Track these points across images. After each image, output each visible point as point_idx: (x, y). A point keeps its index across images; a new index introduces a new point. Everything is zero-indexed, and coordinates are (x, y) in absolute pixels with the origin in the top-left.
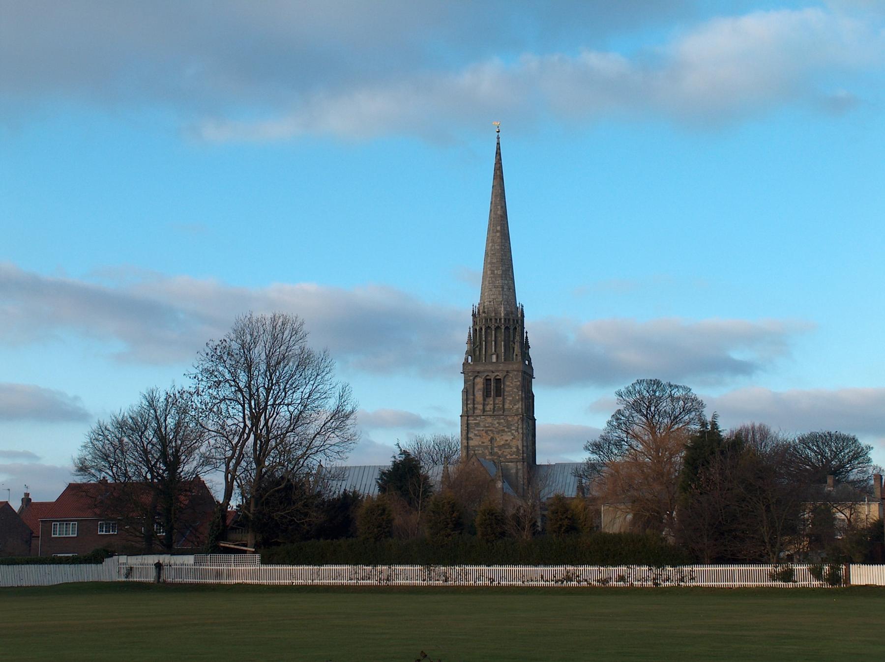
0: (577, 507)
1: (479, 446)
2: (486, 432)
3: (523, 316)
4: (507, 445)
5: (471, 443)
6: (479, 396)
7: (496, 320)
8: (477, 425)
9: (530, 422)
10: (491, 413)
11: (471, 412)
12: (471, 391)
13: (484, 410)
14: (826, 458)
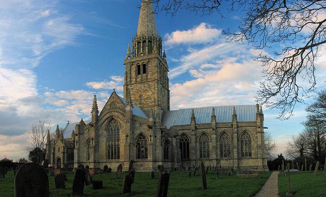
6: (133, 74)
11: (128, 83)
12: (129, 72)
13: (136, 81)
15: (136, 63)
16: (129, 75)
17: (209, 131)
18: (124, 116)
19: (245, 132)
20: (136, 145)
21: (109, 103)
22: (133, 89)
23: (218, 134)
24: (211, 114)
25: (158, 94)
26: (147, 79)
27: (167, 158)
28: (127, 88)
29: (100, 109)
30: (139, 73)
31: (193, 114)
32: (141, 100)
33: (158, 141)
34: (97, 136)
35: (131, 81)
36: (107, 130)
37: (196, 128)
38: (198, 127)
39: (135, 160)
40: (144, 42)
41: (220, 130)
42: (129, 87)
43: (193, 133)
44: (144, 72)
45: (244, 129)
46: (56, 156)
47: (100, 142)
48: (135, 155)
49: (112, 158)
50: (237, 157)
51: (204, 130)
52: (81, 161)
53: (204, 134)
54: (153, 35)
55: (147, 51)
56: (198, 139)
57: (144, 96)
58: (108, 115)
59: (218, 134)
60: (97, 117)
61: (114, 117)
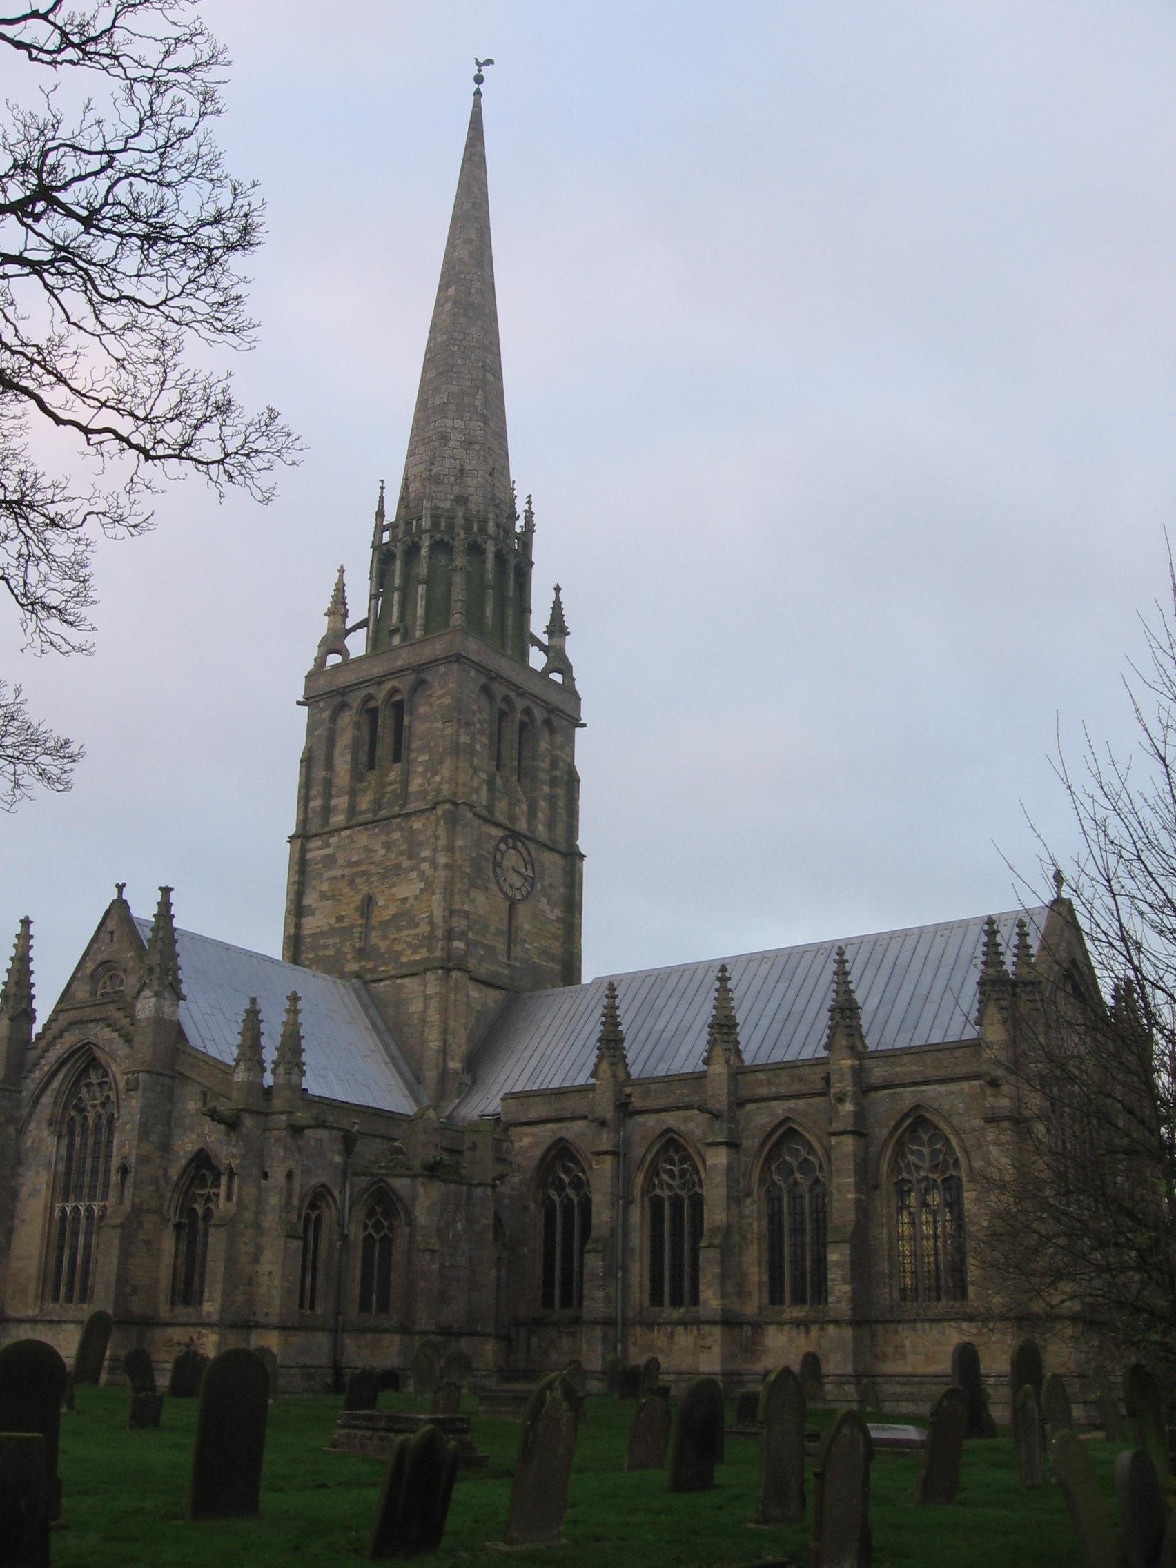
0: (484, 1005)
1: (332, 931)
2: (351, 883)
3: (529, 527)
4: (404, 918)
5: (311, 924)
6: (343, 763)
7: (475, 550)
8: (330, 861)
9: (551, 860)
10: (369, 817)
11: (314, 827)
12: (320, 754)
13: (352, 810)
14: (419, 526)
15: (362, 693)
17: (692, 1125)
18: (129, 1041)
19: (918, 1122)
20: (174, 1219)
21: (90, 967)
23: (751, 1143)
24: (705, 1012)
25: (448, 893)
26: (404, 796)
27: (383, 1307)
28: (303, 851)
29: (44, 1005)
30: (371, 766)
31: (611, 1019)
32: (365, 937)
35: (327, 811)
36: (65, 1127)
37: (625, 1109)
38: (637, 1102)
39: (164, 1312)
40: (442, 547)
41: (761, 1118)
42: (316, 852)
43: (605, 1141)
44: (397, 758)
45: (908, 1097)
47: (24, 1193)
49: (69, 1299)
50: (845, 1309)
53: (671, 1144)
54: (462, 500)
55: (420, 611)
56: (639, 1180)
57: (385, 909)
58: (70, 1040)
59: (751, 1143)
61: (98, 1053)
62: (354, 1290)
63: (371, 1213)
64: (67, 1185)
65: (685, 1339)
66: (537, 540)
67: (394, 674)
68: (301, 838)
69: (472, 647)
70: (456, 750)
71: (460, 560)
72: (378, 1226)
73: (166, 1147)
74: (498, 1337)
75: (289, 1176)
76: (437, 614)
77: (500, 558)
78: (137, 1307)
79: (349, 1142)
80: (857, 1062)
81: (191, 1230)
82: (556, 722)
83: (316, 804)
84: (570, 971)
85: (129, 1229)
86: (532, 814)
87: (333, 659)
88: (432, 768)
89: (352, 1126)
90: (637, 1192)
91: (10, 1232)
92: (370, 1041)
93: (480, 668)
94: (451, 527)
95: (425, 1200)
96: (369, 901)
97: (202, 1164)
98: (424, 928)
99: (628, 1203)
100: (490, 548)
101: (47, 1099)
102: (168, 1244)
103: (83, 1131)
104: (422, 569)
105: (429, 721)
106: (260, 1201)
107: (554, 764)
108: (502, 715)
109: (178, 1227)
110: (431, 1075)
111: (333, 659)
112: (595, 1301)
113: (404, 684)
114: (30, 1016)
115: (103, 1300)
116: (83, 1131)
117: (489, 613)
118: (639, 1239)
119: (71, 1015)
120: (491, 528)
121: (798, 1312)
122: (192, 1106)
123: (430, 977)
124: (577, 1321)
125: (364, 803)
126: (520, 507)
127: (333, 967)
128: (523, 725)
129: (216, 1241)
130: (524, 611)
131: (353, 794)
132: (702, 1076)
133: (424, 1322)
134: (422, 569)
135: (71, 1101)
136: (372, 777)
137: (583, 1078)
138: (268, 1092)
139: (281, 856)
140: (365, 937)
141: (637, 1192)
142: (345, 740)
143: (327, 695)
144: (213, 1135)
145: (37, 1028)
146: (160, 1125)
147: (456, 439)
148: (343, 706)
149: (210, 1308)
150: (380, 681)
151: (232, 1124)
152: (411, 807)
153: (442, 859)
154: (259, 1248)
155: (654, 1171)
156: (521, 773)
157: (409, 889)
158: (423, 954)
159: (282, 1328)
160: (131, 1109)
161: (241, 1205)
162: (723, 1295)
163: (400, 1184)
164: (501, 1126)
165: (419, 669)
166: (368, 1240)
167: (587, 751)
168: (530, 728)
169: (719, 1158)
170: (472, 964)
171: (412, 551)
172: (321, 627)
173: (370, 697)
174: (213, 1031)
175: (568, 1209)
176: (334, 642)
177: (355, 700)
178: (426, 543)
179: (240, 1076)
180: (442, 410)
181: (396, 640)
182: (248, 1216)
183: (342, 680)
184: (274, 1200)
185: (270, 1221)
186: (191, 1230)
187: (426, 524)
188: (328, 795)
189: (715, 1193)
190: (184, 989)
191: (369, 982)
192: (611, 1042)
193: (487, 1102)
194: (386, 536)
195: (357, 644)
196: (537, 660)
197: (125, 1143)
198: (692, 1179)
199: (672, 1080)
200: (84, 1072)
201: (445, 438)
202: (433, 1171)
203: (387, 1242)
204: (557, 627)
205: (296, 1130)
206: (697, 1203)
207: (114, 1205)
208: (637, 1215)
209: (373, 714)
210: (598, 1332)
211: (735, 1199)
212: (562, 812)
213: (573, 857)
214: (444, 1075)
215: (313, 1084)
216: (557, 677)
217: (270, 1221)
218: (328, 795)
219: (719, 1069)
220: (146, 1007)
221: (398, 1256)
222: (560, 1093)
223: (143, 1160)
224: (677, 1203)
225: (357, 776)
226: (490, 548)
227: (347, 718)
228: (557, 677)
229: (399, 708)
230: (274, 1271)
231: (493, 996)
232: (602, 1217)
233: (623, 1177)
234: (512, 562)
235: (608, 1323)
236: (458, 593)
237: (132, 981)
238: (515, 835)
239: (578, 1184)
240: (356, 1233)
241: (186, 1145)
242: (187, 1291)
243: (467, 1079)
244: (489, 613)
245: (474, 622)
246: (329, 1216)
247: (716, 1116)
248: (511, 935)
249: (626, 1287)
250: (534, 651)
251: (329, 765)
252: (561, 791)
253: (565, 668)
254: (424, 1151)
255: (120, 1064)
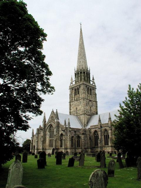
3: (90, 70)
4: (80, 110)
6: (73, 95)
7: (84, 73)
8: (73, 104)
9: (94, 103)
13: (74, 99)
16: (71, 96)
17: (107, 128)
22: (73, 104)
24: (108, 117)
25: (84, 107)
27: (79, 146)
28: (70, 104)
29: (47, 121)
32: (77, 111)
33: (68, 138)
34: (45, 135)
35: (72, 99)
36: (50, 131)
37: (101, 127)
38: (102, 126)
39: (60, 148)
40: (81, 73)
41: (103, 128)
46: (33, 145)
48: (59, 146)
51: (105, 128)
52: (39, 148)
53: (106, 130)
54: (82, 68)
55: (79, 79)
57: (78, 109)
58: (49, 124)
60: (45, 125)
62: (77, 145)
63: (78, 138)
64: (50, 137)
65: (108, 148)
66: (90, 71)
67: (77, 86)
68: (70, 102)
69: (85, 83)
70: (84, 93)
71: (83, 74)
72: (78, 139)
73: (58, 133)
74: (90, 149)
75: (70, 135)
76: (81, 80)
77: (87, 73)
78: (57, 148)
79: (75, 132)
80: (21, 146)
81: (61, 140)
82: (94, 89)
83: (71, 99)
84: (97, 114)
85: (56, 141)
86: (92, 98)
87: (72, 85)
88: (82, 95)
89: (76, 131)
90: (103, 135)
91: (46, 141)
92: (78, 121)
93: (85, 84)
94: (82, 71)
95: (82, 137)
96: (77, 108)
97: (62, 134)
98: (82, 110)
99: (102, 136)
100: (86, 72)
101: (48, 129)
102: (59, 142)
103: (51, 132)
104: (79, 75)
105: (81, 90)
106: (67, 137)
107: (94, 93)
108: (88, 89)
109: (60, 140)
110: (83, 124)
111: (72, 85)
112: (99, 145)
113: (78, 87)
114: (46, 122)
115: (54, 147)
116: (51, 132)
117: (86, 79)
118: (103, 139)
119: (50, 121)
120: (86, 71)
121: (107, 146)
122: (61, 129)
123: (83, 115)
124: (98, 147)
125: (76, 98)
126: (89, 68)
127: (74, 115)
128: (90, 90)
129: (63, 142)
130: (89, 78)
131: (74, 98)
132: (108, 123)
133: (83, 148)
134: (79, 75)
135: (50, 129)
136: (76, 96)
137: (97, 124)
138: (67, 128)
139: (69, 104)
140: (77, 111)
141: (103, 135)
142: (73, 93)
143: (72, 89)
144: (63, 132)
145: (46, 123)
146: (58, 131)
147: (82, 62)
148: (73, 89)
149: (63, 147)
150: (76, 87)
151: (64, 131)
152: (80, 98)
153: (83, 104)
154: (67, 142)
155: (104, 133)
156: (90, 94)
157: (80, 107)
158: (82, 113)
159: (70, 149)
160: (55, 130)
161: (65, 138)
162: (111, 144)
163: (80, 135)
164: (90, 130)
165: (79, 85)
166: (78, 141)
167: (97, 91)
168: (91, 90)
169: (110, 131)
170: (87, 113)
171: (78, 73)
172: (70, 82)
173: (75, 88)
174: (62, 123)
175: (97, 136)
176: (72, 83)
177: (74, 88)
178: (79, 72)
179: (64, 126)
180: (80, 59)
181: (77, 82)
182: (66, 139)
183: (73, 87)
184: (68, 138)
185: (68, 139)
186: (61, 140)
187: (79, 71)
188: (72, 98)
189: (110, 135)
190: (59, 118)
191: (77, 116)
192: (100, 121)
193: (88, 127)
194: (76, 72)
195: (74, 83)
196: (91, 83)
197: (55, 133)
198: (108, 133)
199: (105, 124)
200: (51, 127)
201: (80, 62)
202: (83, 134)
203: (79, 141)
204: (93, 79)
205: (70, 131)
206: (108, 135)
207: (54, 139)
208: (103, 137)
209: (76, 90)
210: (100, 148)
211: (112, 135)
212: (95, 97)
213: (96, 102)
214: (85, 125)
215: (72, 126)
216: (94, 84)
217: (68, 139)
218: (72, 98)
219: (109, 123)
220: (56, 120)
221: (80, 142)
222: (95, 126)
223: (57, 134)
224: (107, 135)
225: (75, 96)
226: (86, 72)
227: (73, 90)
228: (94, 84)
229: (78, 89)
230: (69, 144)
231: (89, 116)
232: (100, 137)
233: (101, 133)
234: (88, 73)
235: (101, 147)
236: (83, 77)
237: (54, 118)
238: (90, 101)
239: (98, 134)
240: (76, 140)
241: (60, 133)
242: (61, 146)
243: (87, 125)
244: (86, 79)
245: (84, 79)
246: (74, 139)
247: (109, 127)
248: (91, 110)
249: (102, 144)
250: (91, 82)
251: (72, 95)
252: (95, 96)
253: (94, 83)
254: (81, 132)
255: (54, 125)
